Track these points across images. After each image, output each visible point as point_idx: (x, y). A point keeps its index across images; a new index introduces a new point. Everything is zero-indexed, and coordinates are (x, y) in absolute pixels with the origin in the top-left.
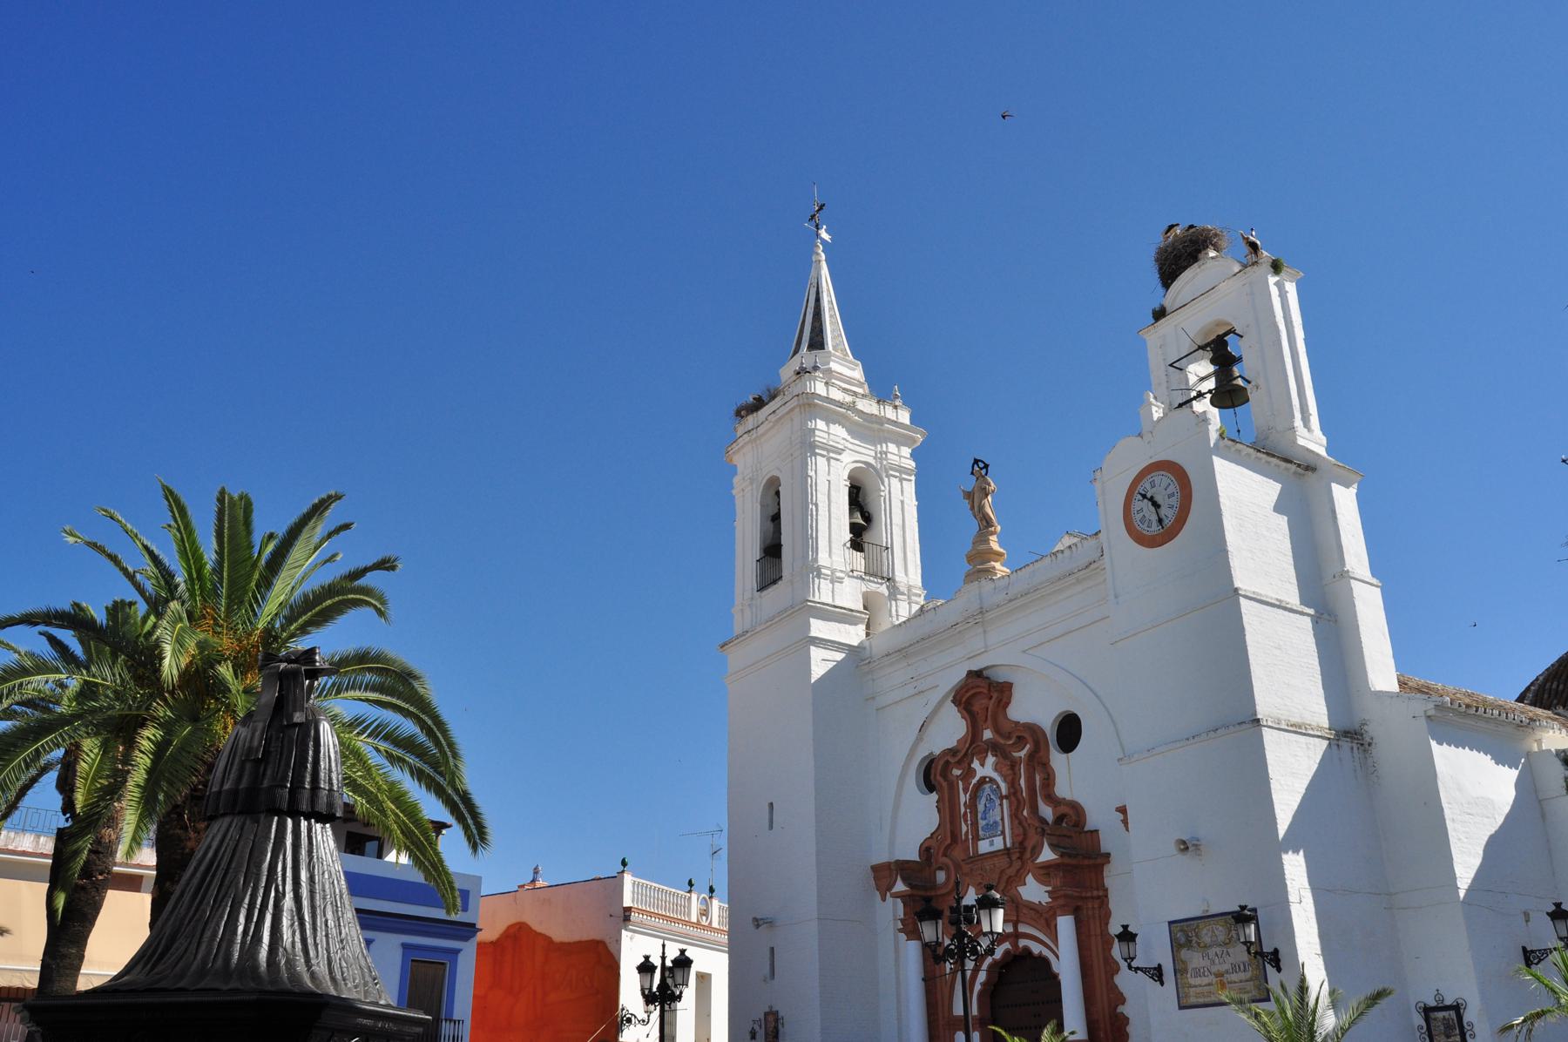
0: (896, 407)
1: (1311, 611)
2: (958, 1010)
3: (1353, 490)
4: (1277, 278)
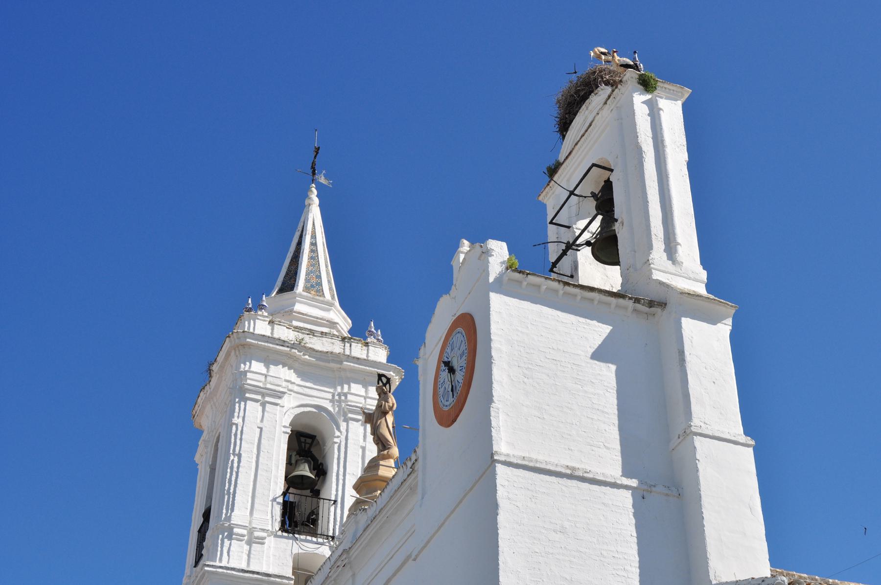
0: (367, 344)
1: (634, 483)
3: (724, 329)
4: (648, 97)
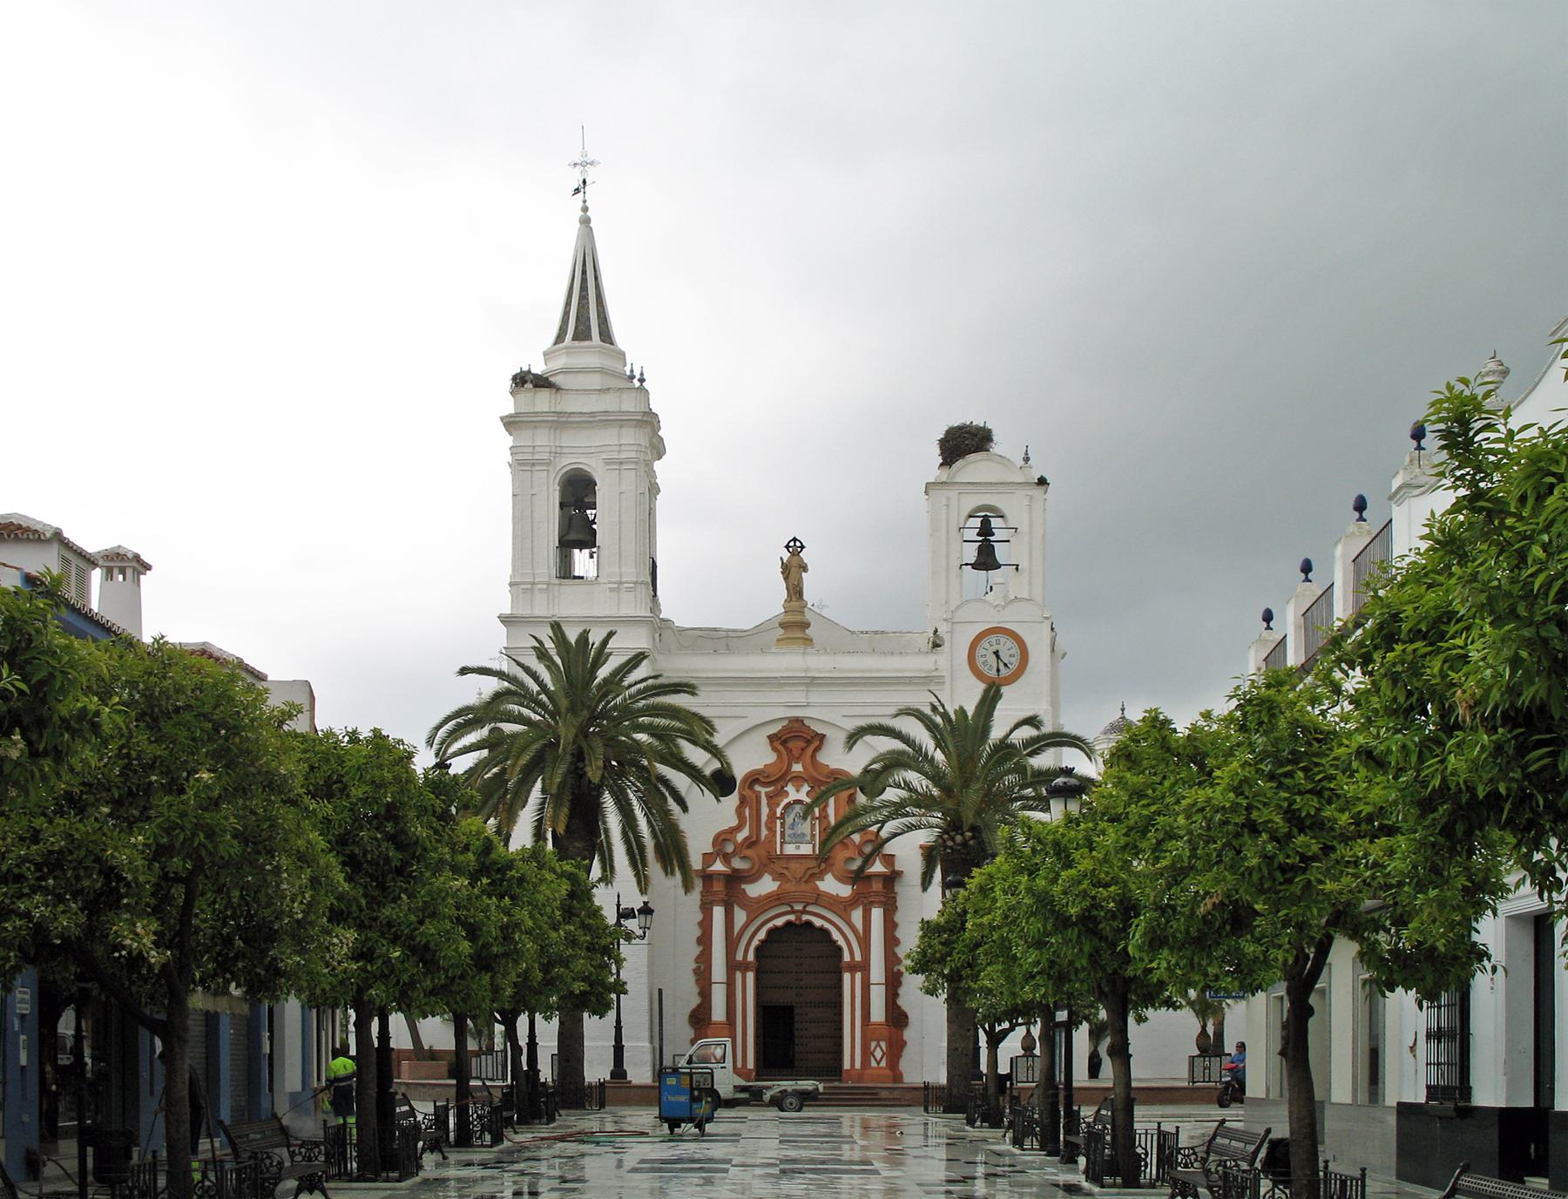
2: (750, 976)
